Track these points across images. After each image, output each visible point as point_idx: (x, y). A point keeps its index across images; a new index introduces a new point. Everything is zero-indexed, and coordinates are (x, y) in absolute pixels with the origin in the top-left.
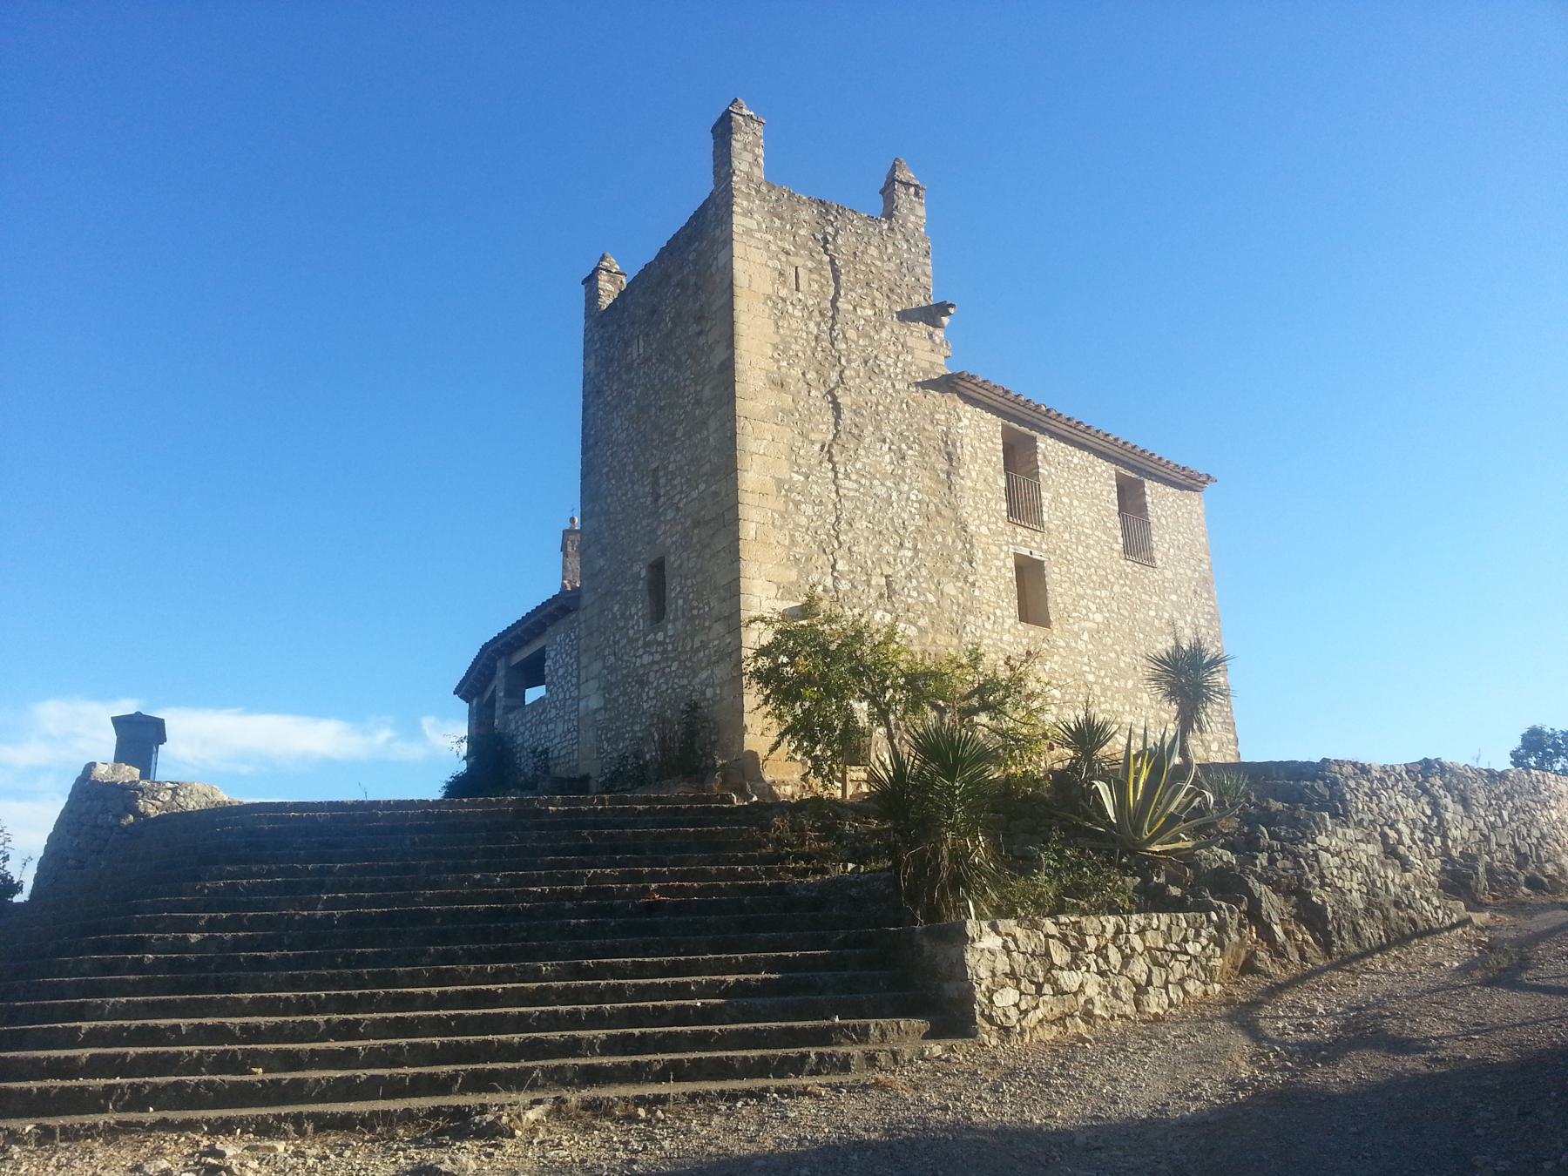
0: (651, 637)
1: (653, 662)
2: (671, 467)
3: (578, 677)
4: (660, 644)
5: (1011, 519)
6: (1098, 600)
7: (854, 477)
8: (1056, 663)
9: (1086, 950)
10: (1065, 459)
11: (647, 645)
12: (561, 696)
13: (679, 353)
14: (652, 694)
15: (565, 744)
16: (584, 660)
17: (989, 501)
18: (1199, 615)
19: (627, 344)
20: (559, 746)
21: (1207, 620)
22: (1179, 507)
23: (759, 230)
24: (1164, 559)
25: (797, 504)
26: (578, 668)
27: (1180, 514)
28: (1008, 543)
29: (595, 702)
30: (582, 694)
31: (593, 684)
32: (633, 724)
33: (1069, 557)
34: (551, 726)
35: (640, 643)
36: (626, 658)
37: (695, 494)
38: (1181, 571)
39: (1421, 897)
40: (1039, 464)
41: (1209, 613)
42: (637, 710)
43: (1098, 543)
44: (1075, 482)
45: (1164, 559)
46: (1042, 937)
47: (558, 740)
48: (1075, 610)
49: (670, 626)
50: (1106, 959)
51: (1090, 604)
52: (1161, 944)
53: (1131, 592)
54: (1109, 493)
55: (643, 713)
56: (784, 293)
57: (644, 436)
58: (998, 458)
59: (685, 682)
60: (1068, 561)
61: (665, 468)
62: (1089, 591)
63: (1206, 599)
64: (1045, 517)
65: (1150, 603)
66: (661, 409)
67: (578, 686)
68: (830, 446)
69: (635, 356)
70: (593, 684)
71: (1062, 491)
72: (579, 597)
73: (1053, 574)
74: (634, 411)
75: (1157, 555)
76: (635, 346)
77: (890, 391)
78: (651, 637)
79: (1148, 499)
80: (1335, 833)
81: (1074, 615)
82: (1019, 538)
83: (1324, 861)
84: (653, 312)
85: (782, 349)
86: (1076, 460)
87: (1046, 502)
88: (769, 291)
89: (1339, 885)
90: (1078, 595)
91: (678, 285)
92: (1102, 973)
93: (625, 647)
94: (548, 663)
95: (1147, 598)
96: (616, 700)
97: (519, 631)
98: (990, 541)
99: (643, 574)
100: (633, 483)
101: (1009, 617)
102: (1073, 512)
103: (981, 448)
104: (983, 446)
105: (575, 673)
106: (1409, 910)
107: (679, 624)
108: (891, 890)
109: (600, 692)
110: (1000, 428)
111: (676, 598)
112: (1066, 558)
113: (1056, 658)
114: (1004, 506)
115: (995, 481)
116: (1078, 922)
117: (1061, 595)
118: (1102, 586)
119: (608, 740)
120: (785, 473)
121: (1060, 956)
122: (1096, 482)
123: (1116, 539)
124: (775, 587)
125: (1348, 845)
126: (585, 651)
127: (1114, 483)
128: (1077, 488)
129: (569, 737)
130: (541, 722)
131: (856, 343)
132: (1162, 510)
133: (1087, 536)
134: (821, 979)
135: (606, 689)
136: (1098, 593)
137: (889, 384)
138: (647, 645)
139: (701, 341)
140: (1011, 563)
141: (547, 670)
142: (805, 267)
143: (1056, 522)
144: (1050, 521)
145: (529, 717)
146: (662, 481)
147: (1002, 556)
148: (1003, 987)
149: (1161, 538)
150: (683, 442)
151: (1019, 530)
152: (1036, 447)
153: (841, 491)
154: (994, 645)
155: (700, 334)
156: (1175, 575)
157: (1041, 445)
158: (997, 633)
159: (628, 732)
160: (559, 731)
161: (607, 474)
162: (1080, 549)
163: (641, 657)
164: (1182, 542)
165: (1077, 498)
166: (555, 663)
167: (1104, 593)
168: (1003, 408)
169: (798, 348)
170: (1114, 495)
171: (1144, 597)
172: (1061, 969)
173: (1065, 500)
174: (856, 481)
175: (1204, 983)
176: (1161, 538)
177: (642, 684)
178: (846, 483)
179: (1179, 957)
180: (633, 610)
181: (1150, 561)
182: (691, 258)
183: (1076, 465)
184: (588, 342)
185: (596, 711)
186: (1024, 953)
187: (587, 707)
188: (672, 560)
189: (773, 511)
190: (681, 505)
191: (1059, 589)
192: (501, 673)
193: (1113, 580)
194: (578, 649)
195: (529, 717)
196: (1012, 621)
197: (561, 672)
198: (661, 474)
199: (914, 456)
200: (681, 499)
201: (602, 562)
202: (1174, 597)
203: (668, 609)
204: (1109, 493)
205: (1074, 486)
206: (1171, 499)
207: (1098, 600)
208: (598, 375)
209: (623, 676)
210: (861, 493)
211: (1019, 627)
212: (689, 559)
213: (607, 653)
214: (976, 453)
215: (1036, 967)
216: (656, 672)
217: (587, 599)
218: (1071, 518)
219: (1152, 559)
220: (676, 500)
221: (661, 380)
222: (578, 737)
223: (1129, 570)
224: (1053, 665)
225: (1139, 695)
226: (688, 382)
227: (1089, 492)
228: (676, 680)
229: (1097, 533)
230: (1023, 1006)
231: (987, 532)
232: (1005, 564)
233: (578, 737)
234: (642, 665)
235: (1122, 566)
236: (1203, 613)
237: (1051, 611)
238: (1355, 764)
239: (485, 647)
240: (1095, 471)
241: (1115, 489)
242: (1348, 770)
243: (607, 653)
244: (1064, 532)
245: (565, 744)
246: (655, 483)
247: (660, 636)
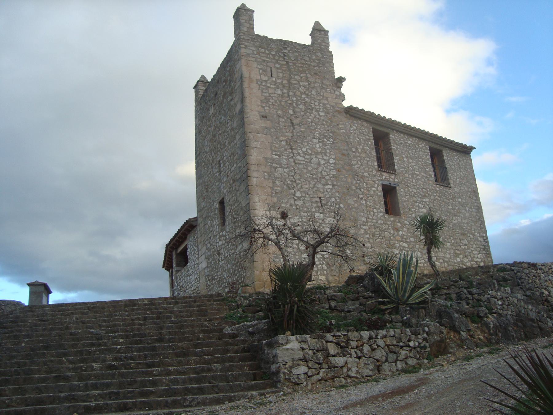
0: (221, 233)
1: (222, 244)
2: (225, 158)
3: (198, 255)
4: (225, 236)
5: (379, 169)
6: (424, 203)
7: (302, 155)
8: (405, 232)
9: (350, 347)
10: (404, 142)
11: (220, 237)
12: (193, 264)
13: (225, 109)
14: (223, 258)
15: (196, 284)
16: (200, 247)
17: (368, 161)
18: (472, 207)
19: (208, 110)
20: (194, 285)
21: (476, 209)
22: (460, 161)
23: (253, 54)
24: (454, 183)
25: (276, 168)
26: (198, 251)
27: (460, 164)
28: (378, 180)
29: (204, 265)
30: (200, 262)
31: (203, 257)
32: (217, 272)
33: (409, 185)
34: (191, 277)
35: (218, 236)
36: (213, 244)
37: (233, 169)
38: (462, 188)
39: (547, 317)
40: (392, 144)
41: (477, 206)
42: (218, 266)
43: (422, 178)
44: (410, 152)
45: (454, 183)
46: (324, 343)
47: (193, 283)
48: (413, 208)
49: (227, 227)
50: (361, 351)
51: (420, 205)
52: (395, 343)
53: (439, 199)
54: (426, 156)
55: (220, 267)
56: (266, 78)
57: (215, 147)
58: (372, 143)
59: (233, 251)
60: (408, 186)
61: (223, 159)
62: (419, 199)
63: (475, 200)
64: (396, 167)
65: (449, 203)
66: (220, 134)
67: (198, 258)
68: (290, 142)
69: (211, 114)
70: (203, 257)
71: (404, 156)
72: (197, 220)
73: (401, 192)
74: (212, 137)
75: (451, 182)
76: (211, 110)
77: (317, 116)
78: (221, 233)
79: (445, 158)
80: (499, 290)
81: (412, 210)
82: (384, 177)
83: (493, 302)
84: (216, 94)
85: (266, 101)
86: (409, 142)
87: (396, 161)
88: (259, 78)
89: (501, 313)
90: (414, 201)
91: (224, 82)
92: (359, 358)
93: (213, 239)
94: (189, 250)
95: (447, 201)
96: (211, 263)
97: (177, 238)
98: (369, 179)
99: (217, 206)
100: (212, 168)
101: (381, 212)
102: (410, 165)
103: (362, 139)
104: (364, 138)
105: (197, 253)
106: (540, 323)
107: (230, 226)
108: (266, 327)
109: (206, 260)
110: (372, 130)
111: (229, 215)
112: (407, 185)
113: (405, 229)
114: (376, 164)
115: (371, 153)
116: (347, 335)
117: (405, 201)
118: (425, 196)
119: (209, 280)
120: (269, 155)
121: (332, 349)
122: (420, 151)
123: (431, 176)
124: (267, 205)
125: (506, 295)
126: (200, 243)
127: (429, 151)
128: (411, 154)
129: (196, 281)
130: (188, 276)
131: (301, 97)
132: (452, 162)
133: (417, 175)
134: (214, 366)
135: (208, 258)
136: (424, 200)
137: (317, 114)
138: (220, 237)
139: (232, 103)
140: (380, 189)
141: (188, 253)
142: (275, 67)
143: (402, 169)
144: (399, 169)
145: (184, 274)
146: (222, 165)
147: (376, 185)
148: (298, 365)
149: (452, 174)
150: (228, 147)
151: (383, 174)
152: (389, 137)
153: (296, 161)
154: (374, 225)
155: (231, 100)
156: (460, 190)
157: (392, 136)
158: (375, 220)
159: (216, 276)
160: (193, 279)
161: (204, 166)
162: (414, 181)
163: (218, 243)
164: (463, 175)
165: (411, 159)
166: (190, 250)
167: (427, 200)
168: (420, 136)
169: (273, 101)
170: (429, 157)
171: (445, 200)
172: (334, 356)
173: (405, 159)
174: (303, 157)
175: (418, 359)
176: (452, 174)
177: (219, 254)
178: (298, 158)
179: (405, 348)
180: (215, 223)
181: (448, 186)
182: (228, 69)
183: (410, 144)
184: (196, 111)
185: (205, 269)
186: (312, 350)
187: (202, 267)
188: (227, 199)
189: (264, 172)
190: (229, 174)
191: (405, 199)
192: (174, 257)
193: (430, 194)
194: (198, 243)
195: (184, 274)
196: (382, 214)
197: (193, 253)
198: (221, 162)
199: (331, 144)
200: (228, 172)
201: (204, 204)
202: (460, 200)
203: (226, 220)
204: (426, 156)
205: (409, 154)
206: (456, 158)
207: (424, 203)
208: (199, 125)
209: (213, 252)
210: (306, 162)
211: (386, 217)
212: (232, 197)
213: (207, 243)
214: (361, 141)
215: (320, 356)
216: (224, 248)
217: (200, 220)
218: (409, 168)
219: (449, 184)
220: (226, 173)
221: (220, 122)
222: (199, 280)
223: (438, 189)
224: (403, 233)
225: (446, 243)
226: (228, 121)
227: (417, 156)
228: (231, 251)
229: (422, 174)
230: (310, 374)
231: (368, 175)
232: (377, 190)
233: (199, 280)
234: (219, 246)
235: (434, 187)
236: (474, 206)
237: (401, 209)
238: (529, 264)
239: (167, 246)
240: (420, 147)
241: (429, 154)
242: (526, 266)
243: (207, 243)
244: (405, 174)
245: (196, 284)
246: (220, 164)
247: (224, 233)
